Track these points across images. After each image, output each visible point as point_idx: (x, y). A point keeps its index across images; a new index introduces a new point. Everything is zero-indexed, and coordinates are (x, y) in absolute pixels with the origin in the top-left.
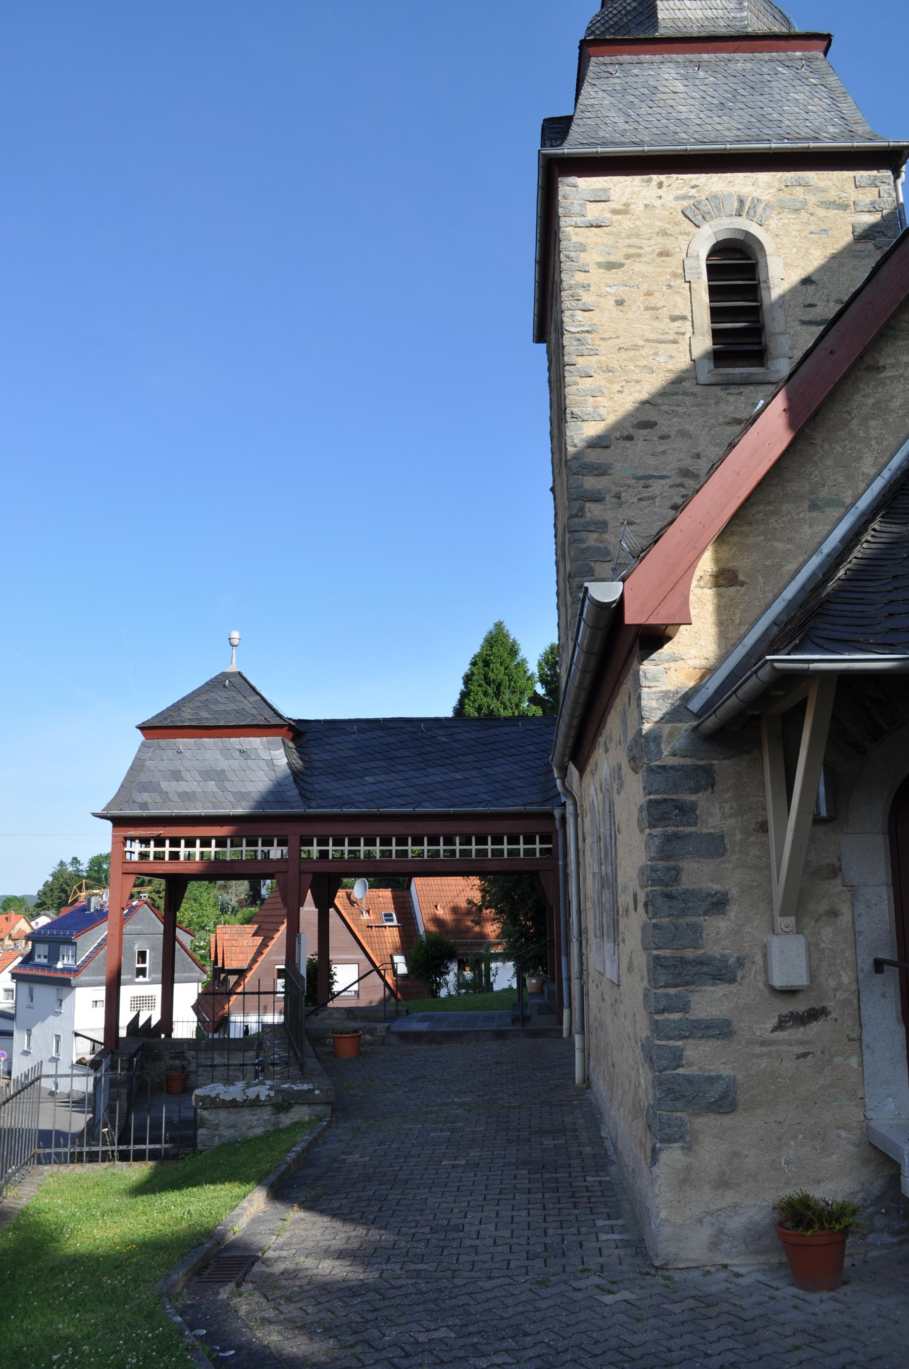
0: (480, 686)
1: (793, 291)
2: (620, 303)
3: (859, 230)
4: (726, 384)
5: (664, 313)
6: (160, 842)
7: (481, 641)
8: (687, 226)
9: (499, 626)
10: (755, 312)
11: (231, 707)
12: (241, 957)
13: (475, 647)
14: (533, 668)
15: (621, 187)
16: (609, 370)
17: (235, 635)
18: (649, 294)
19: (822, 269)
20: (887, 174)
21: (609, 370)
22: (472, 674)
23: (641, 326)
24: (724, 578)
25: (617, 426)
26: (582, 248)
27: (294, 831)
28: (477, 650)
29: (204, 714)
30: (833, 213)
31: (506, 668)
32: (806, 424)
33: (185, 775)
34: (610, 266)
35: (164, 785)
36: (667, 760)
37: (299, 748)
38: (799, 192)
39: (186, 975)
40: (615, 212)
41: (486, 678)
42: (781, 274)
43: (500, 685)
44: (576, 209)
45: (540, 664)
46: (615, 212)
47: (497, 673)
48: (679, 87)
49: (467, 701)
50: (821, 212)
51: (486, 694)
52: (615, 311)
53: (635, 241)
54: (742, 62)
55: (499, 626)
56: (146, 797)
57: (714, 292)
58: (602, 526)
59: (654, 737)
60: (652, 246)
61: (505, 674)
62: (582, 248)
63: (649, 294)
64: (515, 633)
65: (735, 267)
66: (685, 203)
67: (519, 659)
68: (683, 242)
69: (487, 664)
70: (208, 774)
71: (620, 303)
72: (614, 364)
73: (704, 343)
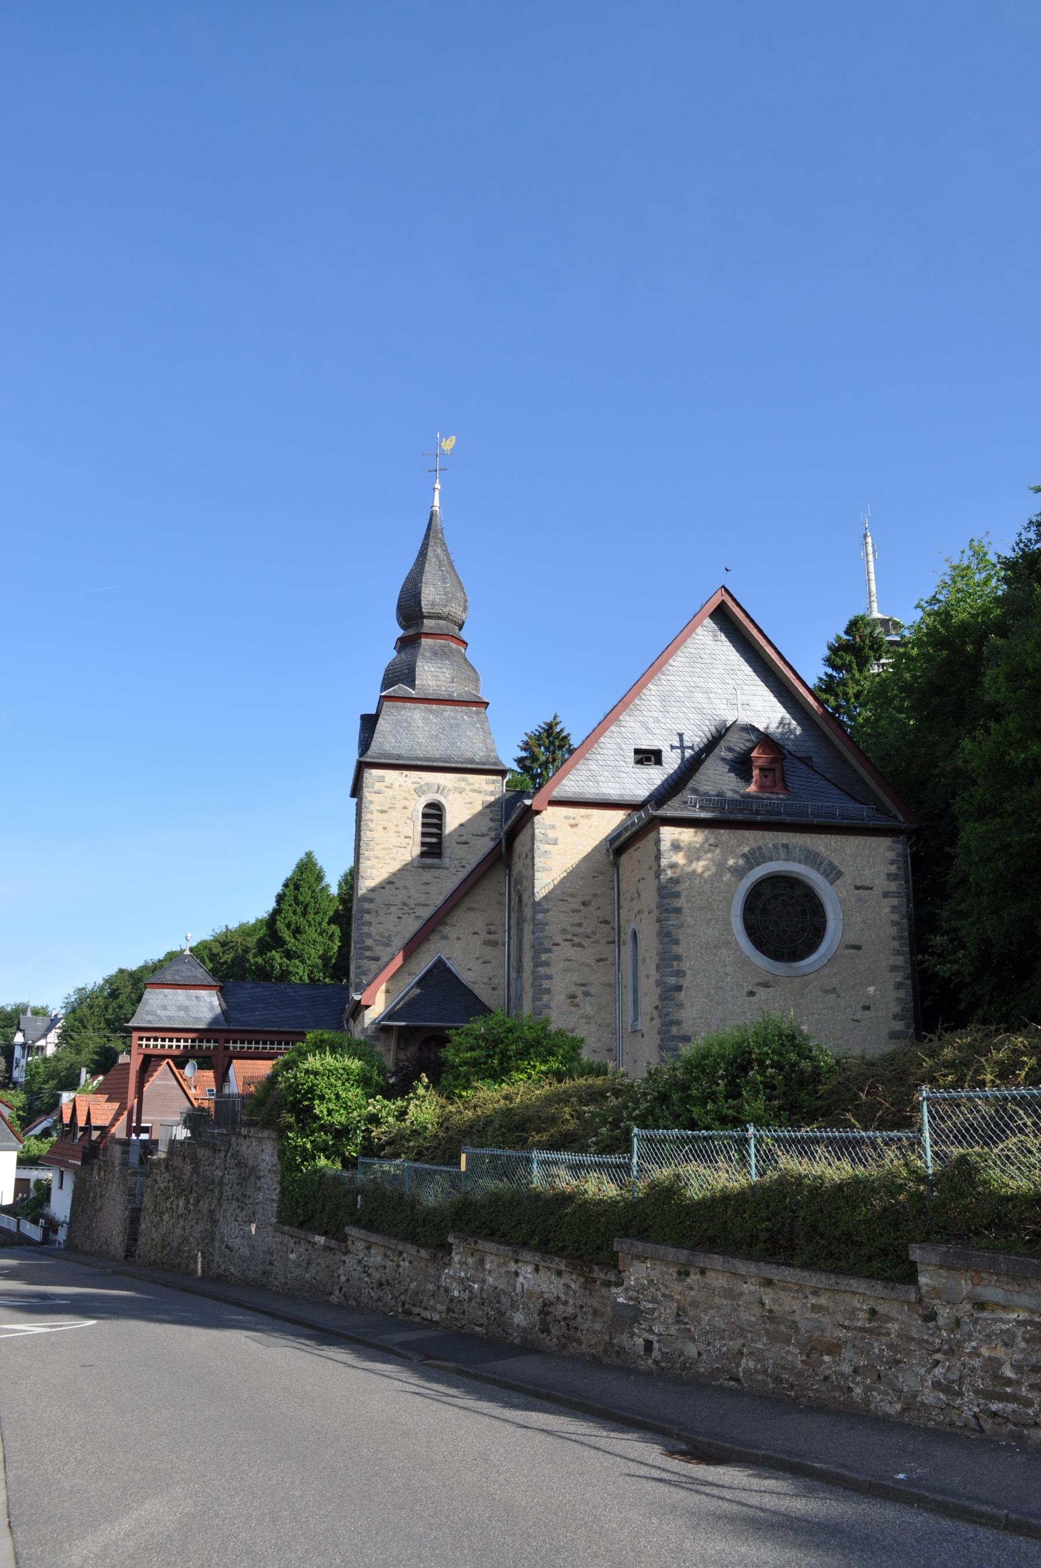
0: (290, 905)
1: (456, 830)
2: (385, 828)
3: (485, 805)
4: (425, 867)
5: (402, 835)
6: (156, 1039)
7: (293, 867)
8: (415, 796)
9: (309, 855)
10: (439, 836)
11: (189, 974)
12: (103, 1117)
13: (287, 870)
14: (334, 890)
15: (391, 776)
16: (378, 858)
17: (189, 935)
18: (397, 826)
19: (470, 820)
20: (500, 778)
21: (378, 858)
22: (284, 895)
23: (392, 840)
24: (387, 991)
25: (381, 883)
26: (371, 802)
27: (222, 1037)
28: (289, 874)
29: (177, 978)
30: (476, 794)
31: (313, 891)
32: (406, 958)
33: (169, 1008)
34: (382, 812)
35: (159, 1012)
36: (369, 1033)
37: (223, 995)
38: (463, 784)
39: (4, 1144)
40: (387, 787)
41: (296, 899)
42: (452, 822)
43: (307, 906)
44: (370, 785)
45: (340, 885)
46: (387, 787)
47: (305, 896)
48: (421, 724)
49: (278, 918)
50: (471, 794)
51: (294, 912)
52: (383, 832)
53: (393, 801)
54: (449, 711)
55: (309, 855)
56: (150, 1018)
57: (424, 825)
58: (370, 924)
59: (367, 1028)
60: (400, 804)
61: (312, 897)
62: (371, 802)
63: (397, 826)
64: (322, 861)
65: (434, 813)
66: (416, 785)
67: (323, 884)
68: (413, 803)
69: (297, 887)
70: (180, 1008)
71: (385, 828)
72: (380, 856)
73: (417, 850)
